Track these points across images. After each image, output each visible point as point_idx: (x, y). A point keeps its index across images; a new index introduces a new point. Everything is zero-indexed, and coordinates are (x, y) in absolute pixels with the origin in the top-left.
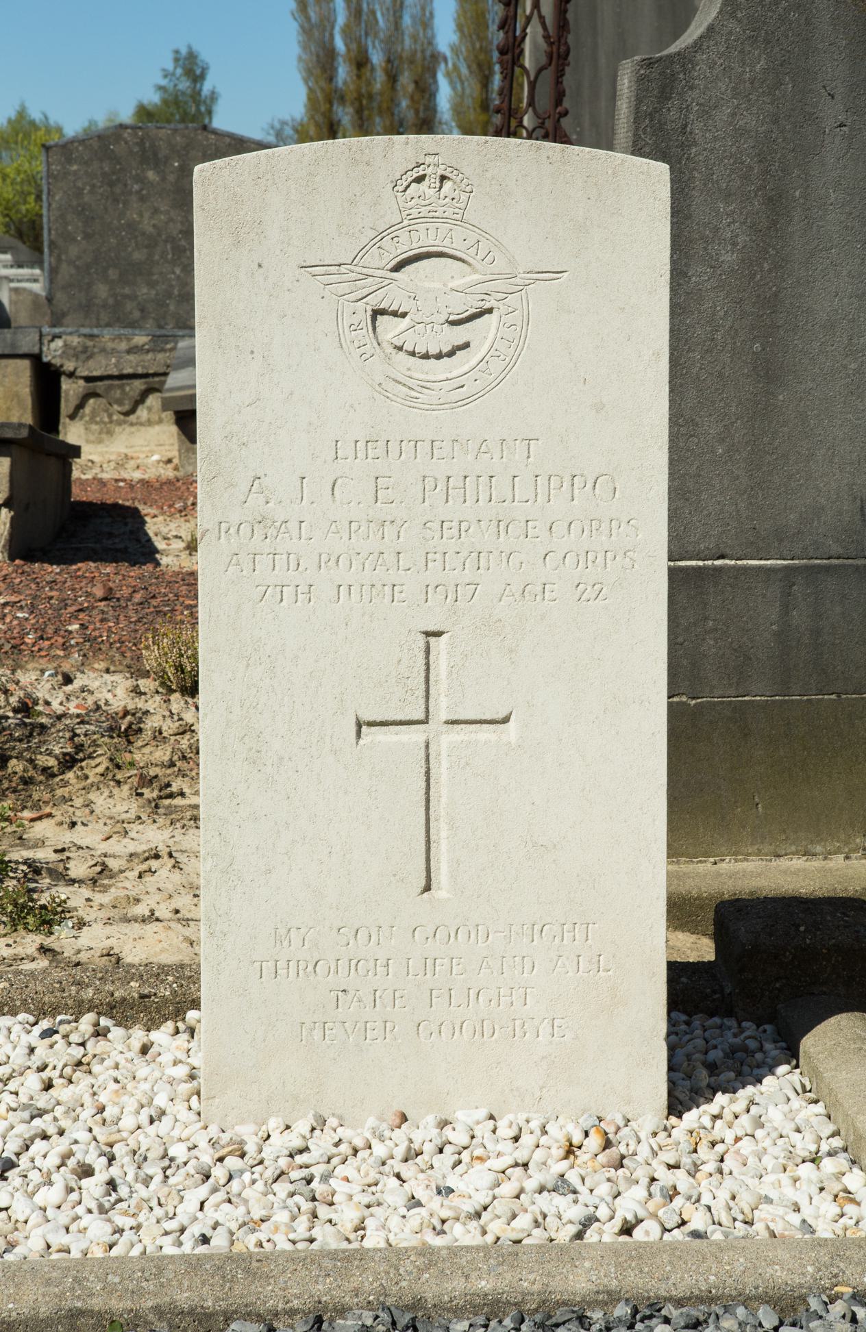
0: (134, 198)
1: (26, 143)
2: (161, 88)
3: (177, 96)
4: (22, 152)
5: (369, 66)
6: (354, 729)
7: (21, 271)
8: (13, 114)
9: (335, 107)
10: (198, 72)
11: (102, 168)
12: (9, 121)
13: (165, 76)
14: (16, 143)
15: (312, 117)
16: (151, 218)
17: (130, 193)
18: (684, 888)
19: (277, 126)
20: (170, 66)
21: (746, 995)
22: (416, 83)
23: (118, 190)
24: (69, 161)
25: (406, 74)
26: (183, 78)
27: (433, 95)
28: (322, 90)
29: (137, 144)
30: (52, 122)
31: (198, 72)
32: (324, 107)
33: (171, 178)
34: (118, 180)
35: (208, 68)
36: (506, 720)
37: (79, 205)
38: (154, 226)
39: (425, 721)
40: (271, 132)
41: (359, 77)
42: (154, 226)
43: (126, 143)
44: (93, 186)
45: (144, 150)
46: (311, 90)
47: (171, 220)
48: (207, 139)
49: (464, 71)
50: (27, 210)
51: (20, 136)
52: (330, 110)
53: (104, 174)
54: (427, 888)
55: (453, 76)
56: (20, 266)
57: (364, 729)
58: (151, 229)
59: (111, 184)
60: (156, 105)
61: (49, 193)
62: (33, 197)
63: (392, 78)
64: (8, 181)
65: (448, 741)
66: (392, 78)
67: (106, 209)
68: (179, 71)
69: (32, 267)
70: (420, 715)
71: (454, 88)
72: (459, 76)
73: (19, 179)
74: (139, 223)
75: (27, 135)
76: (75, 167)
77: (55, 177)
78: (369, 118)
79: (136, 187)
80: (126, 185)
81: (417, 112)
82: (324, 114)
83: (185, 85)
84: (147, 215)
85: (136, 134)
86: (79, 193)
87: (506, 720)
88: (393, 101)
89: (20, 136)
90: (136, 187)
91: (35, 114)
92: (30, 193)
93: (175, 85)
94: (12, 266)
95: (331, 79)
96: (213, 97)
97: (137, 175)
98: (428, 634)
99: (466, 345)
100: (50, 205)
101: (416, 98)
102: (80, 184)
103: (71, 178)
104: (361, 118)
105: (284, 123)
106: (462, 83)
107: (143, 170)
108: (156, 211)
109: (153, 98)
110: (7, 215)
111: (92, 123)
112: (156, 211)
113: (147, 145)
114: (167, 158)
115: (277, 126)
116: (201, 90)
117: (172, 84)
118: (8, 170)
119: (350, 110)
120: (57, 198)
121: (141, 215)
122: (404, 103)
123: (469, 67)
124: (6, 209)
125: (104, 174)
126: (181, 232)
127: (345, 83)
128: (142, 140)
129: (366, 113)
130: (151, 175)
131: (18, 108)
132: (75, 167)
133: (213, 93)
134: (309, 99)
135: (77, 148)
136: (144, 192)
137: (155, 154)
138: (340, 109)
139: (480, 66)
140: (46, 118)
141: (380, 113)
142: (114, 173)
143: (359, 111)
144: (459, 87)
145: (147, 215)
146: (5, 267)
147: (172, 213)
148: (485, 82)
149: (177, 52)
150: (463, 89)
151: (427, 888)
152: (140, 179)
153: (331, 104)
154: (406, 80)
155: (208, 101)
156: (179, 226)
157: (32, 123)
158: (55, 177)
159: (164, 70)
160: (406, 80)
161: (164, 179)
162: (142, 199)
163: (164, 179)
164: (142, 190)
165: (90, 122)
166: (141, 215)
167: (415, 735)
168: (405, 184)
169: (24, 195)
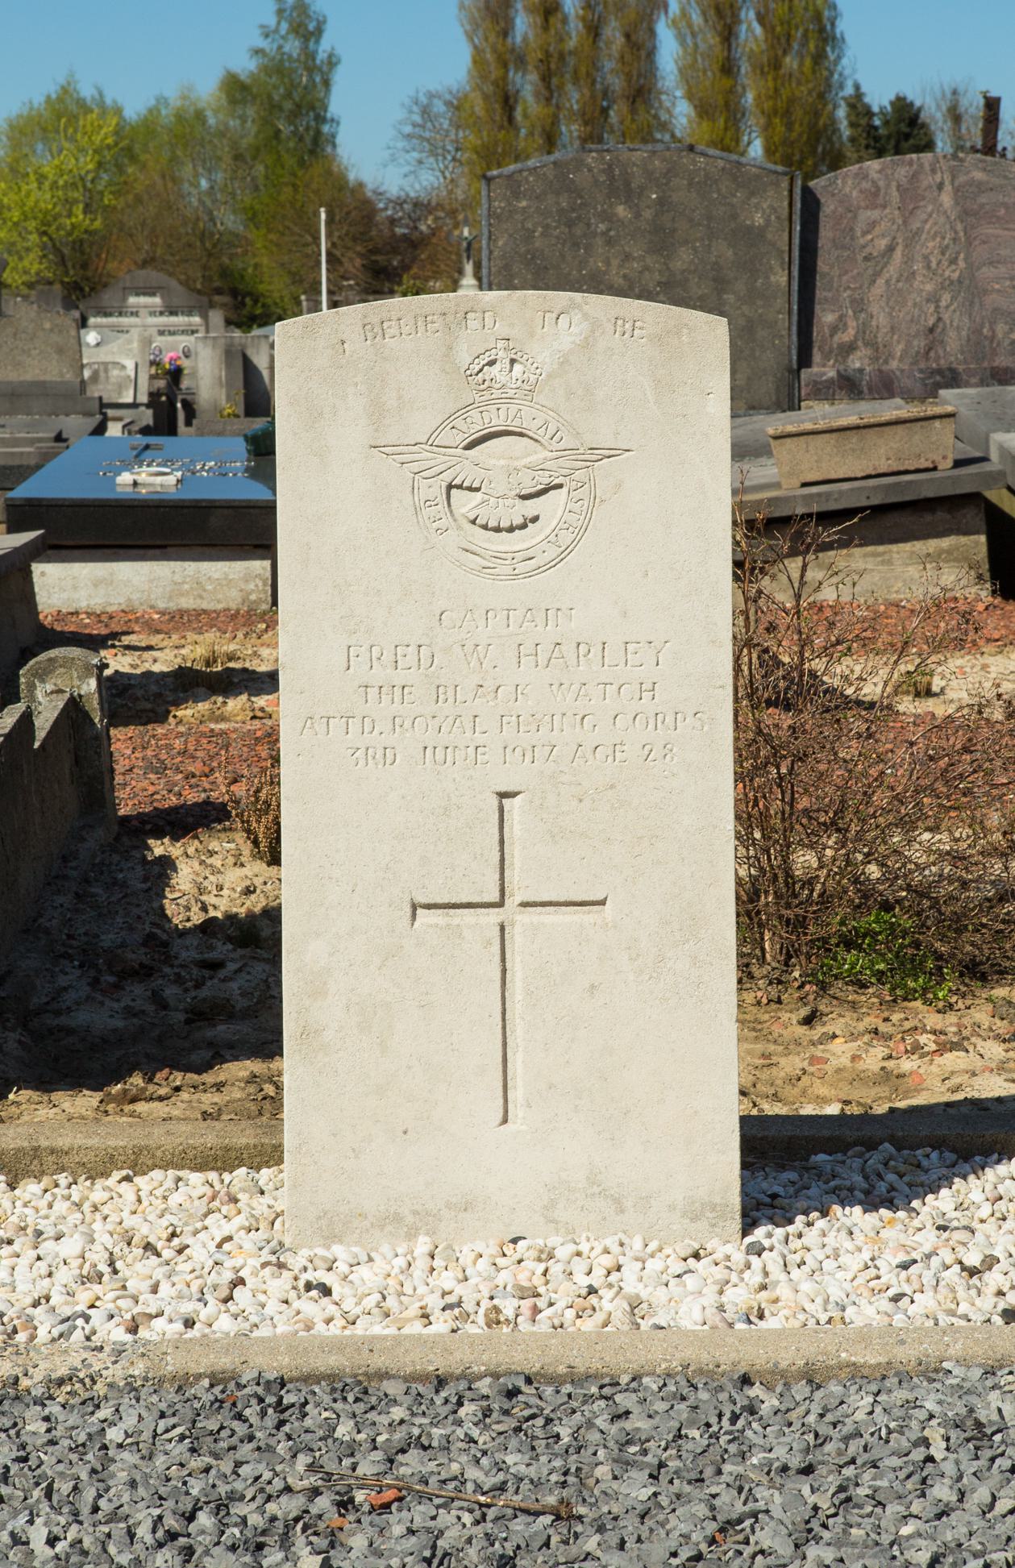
0: (599, 241)
1: (71, 130)
2: (258, 52)
3: (281, 61)
4: (66, 145)
5: (560, 16)
6: (408, 910)
7: (173, 319)
8: (53, 90)
9: (511, 74)
10: (311, 26)
11: (558, 203)
12: (48, 97)
13: (267, 36)
14: (57, 132)
15: (478, 87)
16: (621, 266)
17: (594, 234)
18: (764, 1120)
19: (424, 100)
20: (271, 21)
21: (791, 1164)
22: (628, 36)
23: (578, 231)
24: (517, 195)
25: (614, 24)
26: (291, 36)
27: (651, 54)
28: (494, 50)
29: (603, 171)
30: (108, 101)
31: (311, 26)
32: (495, 73)
33: (648, 214)
34: (579, 218)
35: (325, 22)
36: (603, 903)
37: (528, 251)
38: (625, 276)
39: (500, 904)
40: (415, 108)
41: (546, 27)
42: (625, 276)
43: (590, 170)
44: (547, 227)
45: (612, 178)
46: (478, 53)
47: (647, 268)
48: (694, 162)
49: (697, 18)
50: (73, 226)
51: (63, 120)
52: (505, 78)
53: (561, 211)
54: (505, 1121)
55: (683, 27)
56: (173, 313)
57: (419, 911)
58: (621, 281)
59: (570, 224)
60: (252, 73)
61: (490, 238)
62: (81, 206)
63: (594, 30)
64: (47, 184)
65: (522, 922)
66: (594, 30)
67: (563, 256)
68: (284, 26)
69: (190, 314)
70: (494, 896)
71: (682, 42)
72: (690, 26)
73: (61, 183)
74: (605, 273)
75: (73, 119)
76: (524, 203)
77: (498, 217)
78: (561, 87)
79: (602, 227)
80: (588, 225)
81: (628, 75)
82: (495, 83)
83: (293, 47)
84: (615, 262)
85: (603, 158)
86: (529, 236)
87: (603, 903)
88: (594, 64)
89: (63, 120)
90: (602, 227)
91: (87, 92)
92: (76, 201)
93: (280, 47)
94: (161, 313)
95: (505, 33)
96: (332, 62)
97: (604, 211)
98: (503, 795)
99: (535, 519)
100: (491, 252)
101: (628, 57)
102: (530, 225)
103: (518, 217)
104: (548, 87)
105: (431, 96)
106: (694, 35)
107: (611, 206)
108: (627, 257)
109: (245, 65)
110: (45, 233)
111: (162, 100)
112: (627, 257)
113: (617, 172)
114: (642, 188)
115: (424, 100)
116: (315, 52)
117: (275, 46)
118: (46, 169)
119: (533, 77)
120: (500, 243)
121: (608, 263)
122: (608, 65)
123: (704, 13)
124: (43, 224)
125: (561, 211)
126: (659, 283)
127: (525, 39)
128: (610, 166)
129: (555, 81)
130: (621, 211)
131: (63, 82)
132: (524, 203)
133: (330, 56)
134: (475, 62)
135: (526, 179)
136: (612, 233)
137: (627, 184)
138: (518, 78)
139: (718, 10)
140: (101, 94)
141: (576, 79)
142: (573, 210)
143: (546, 78)
144: (689, 40)
145: (615, 262)
146: (152, 314)
147: (649, 260)
148: (728, 35)
149: (403, 105)
150: (696, 45)
151: (505, 1121)
152: (608, 217)
153: (505, 66)
154: (613, 33)
155: (325, 68)
156: (657, 276)
157: (81, 104)
158: (498, 217)
159: (262, 26)
160: (613, 33)
161: (638, 215)
162: (610, 242)
163: (638, 215)
164: (609, 230)
165: (157, 100)
166: (608, 263)
167: (493, 917)
168: (477, 368)
169: (69, 203)
